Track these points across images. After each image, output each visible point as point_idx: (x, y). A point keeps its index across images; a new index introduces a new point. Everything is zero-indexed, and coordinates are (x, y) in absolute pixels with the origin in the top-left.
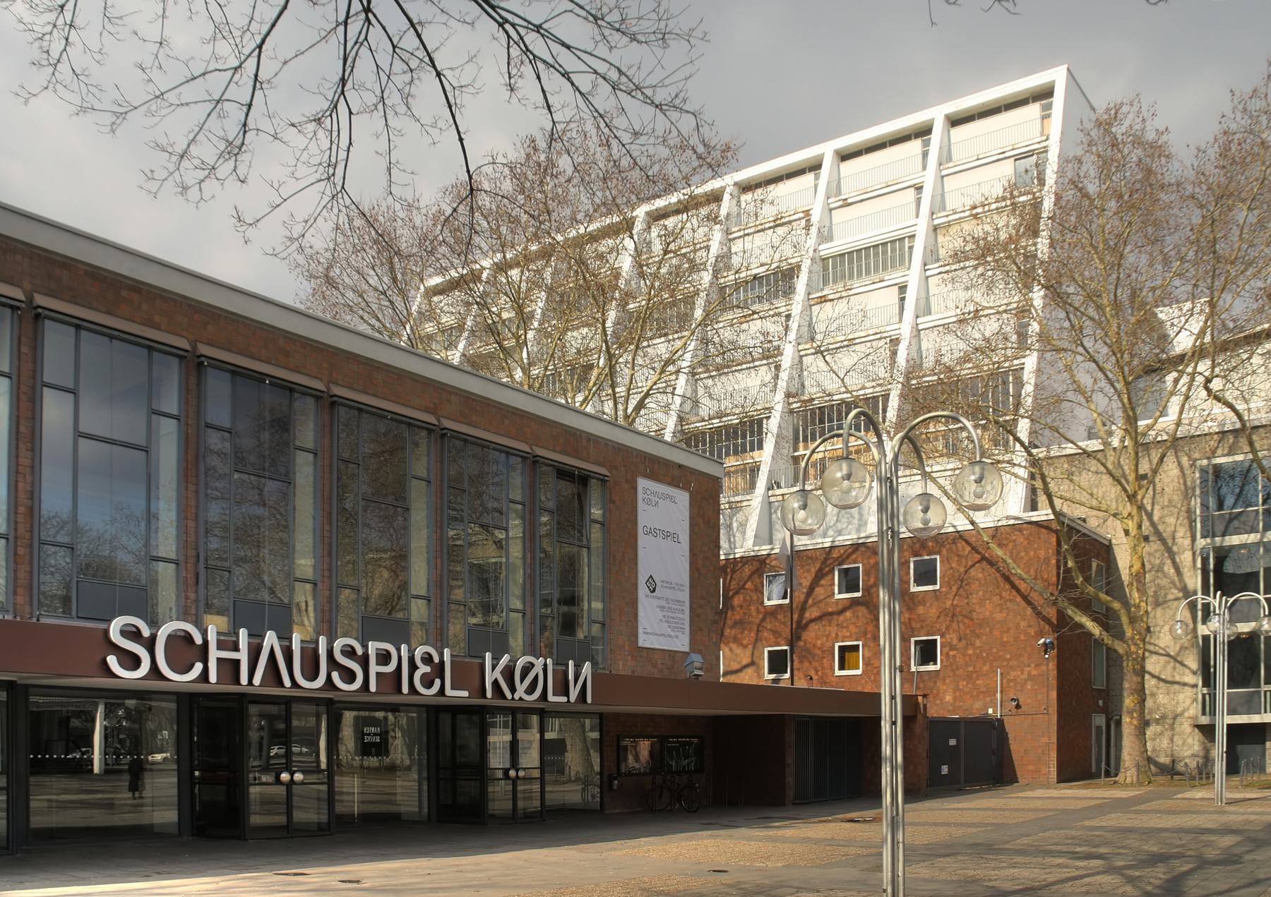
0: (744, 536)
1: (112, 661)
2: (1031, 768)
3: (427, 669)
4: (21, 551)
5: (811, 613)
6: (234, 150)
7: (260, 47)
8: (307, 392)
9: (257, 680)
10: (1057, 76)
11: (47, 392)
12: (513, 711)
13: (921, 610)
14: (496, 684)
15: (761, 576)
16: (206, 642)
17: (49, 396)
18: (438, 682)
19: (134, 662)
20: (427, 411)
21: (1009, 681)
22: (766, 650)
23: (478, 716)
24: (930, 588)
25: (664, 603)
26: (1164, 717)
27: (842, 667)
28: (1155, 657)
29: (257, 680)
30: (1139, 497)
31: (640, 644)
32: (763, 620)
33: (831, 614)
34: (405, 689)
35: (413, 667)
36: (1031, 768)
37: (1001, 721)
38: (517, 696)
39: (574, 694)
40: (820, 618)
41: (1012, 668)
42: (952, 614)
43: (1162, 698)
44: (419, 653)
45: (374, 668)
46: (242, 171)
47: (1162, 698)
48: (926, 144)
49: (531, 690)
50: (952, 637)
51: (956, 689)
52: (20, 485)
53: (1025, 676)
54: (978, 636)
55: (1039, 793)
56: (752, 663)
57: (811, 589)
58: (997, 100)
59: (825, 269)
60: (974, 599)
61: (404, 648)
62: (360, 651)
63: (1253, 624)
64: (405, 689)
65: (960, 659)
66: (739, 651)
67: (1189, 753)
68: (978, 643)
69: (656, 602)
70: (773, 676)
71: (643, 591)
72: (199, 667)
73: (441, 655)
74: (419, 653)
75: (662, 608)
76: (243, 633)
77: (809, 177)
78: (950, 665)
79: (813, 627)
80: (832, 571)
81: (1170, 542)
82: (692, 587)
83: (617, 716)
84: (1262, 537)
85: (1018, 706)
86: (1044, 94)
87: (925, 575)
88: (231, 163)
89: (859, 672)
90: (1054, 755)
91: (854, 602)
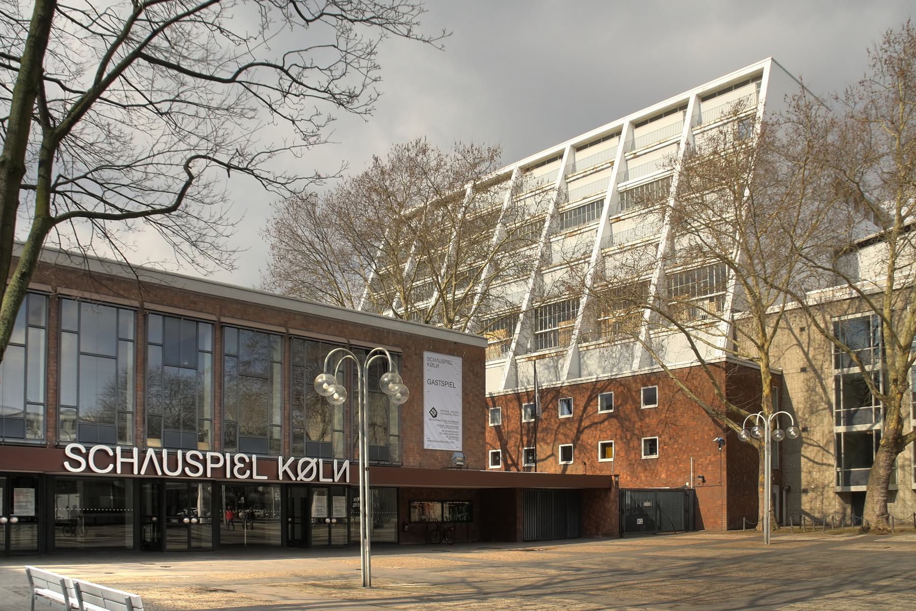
0: (496, 381)
1: (67, 464)
2: (711, 520)
3: (242, 465)
4: (51, 411)
5: (585, 423)
8: (206, 321)
9: (143, 472)
10: (766, 65)
11: (63, 334)
13: (647, 420)
14: (285, 472)
15: (557, 400)
16: (115, 455)
17: (65, 336)
18: (248, 472)
19: (78, 464)
20: (280, 325)
21: (699, 465)
22: (560, 446)
24: (653, 406)
25: (443, 423)
26: (817, 487)
27: (604, 456)
28: (811, 448)
29: (143, 472)
30: (766, 347)
31: (425, 447)
32: (559, 427)
33: (596, 423)
34: (228, 476)
35: (233, 464)
36: (711, 520)
37: (694, 491)
38: (299, 479)
39: (337, 478)
40: (590, 426)
41: (700, 457)
42: (665, 423)
43: (815, 475)
44: (237, 457)
45: (210, 466)
47: (815, 475)
48: (759, 86)
49: (309, 475)
50: (665, 437)
51: (668, 470)
52: (51, 380)
53: (707, 462)
54: (680, 437)
56: (553, 455)
57: (585, 409)
58: (728, 83)
59: (622, 199)
60: (678, 413)
61: (228, 456)
63: (869, 425)
64: (228, 476)
65: (670, 452)
66: (545, 447)
67: (832, 511)
68: (680, 441)
69: (436, 423)
70: (564, 463)
71: (427, 417)
72: (111, 466)
73: (250, 459)
74: (237, 457)
75: (441, 426)
77: (680, 114)
78: (664, 454)
79: (586, 431)
80: (597, 397)
81: (819, 371)
82: (464, 413)
83: (402, 488)
84: (873, 367)
85: (704, 481)
86: (756, 77)
87: (650, 399)
89: (611, 460)
90: (725, 512)
91: (610, 416)
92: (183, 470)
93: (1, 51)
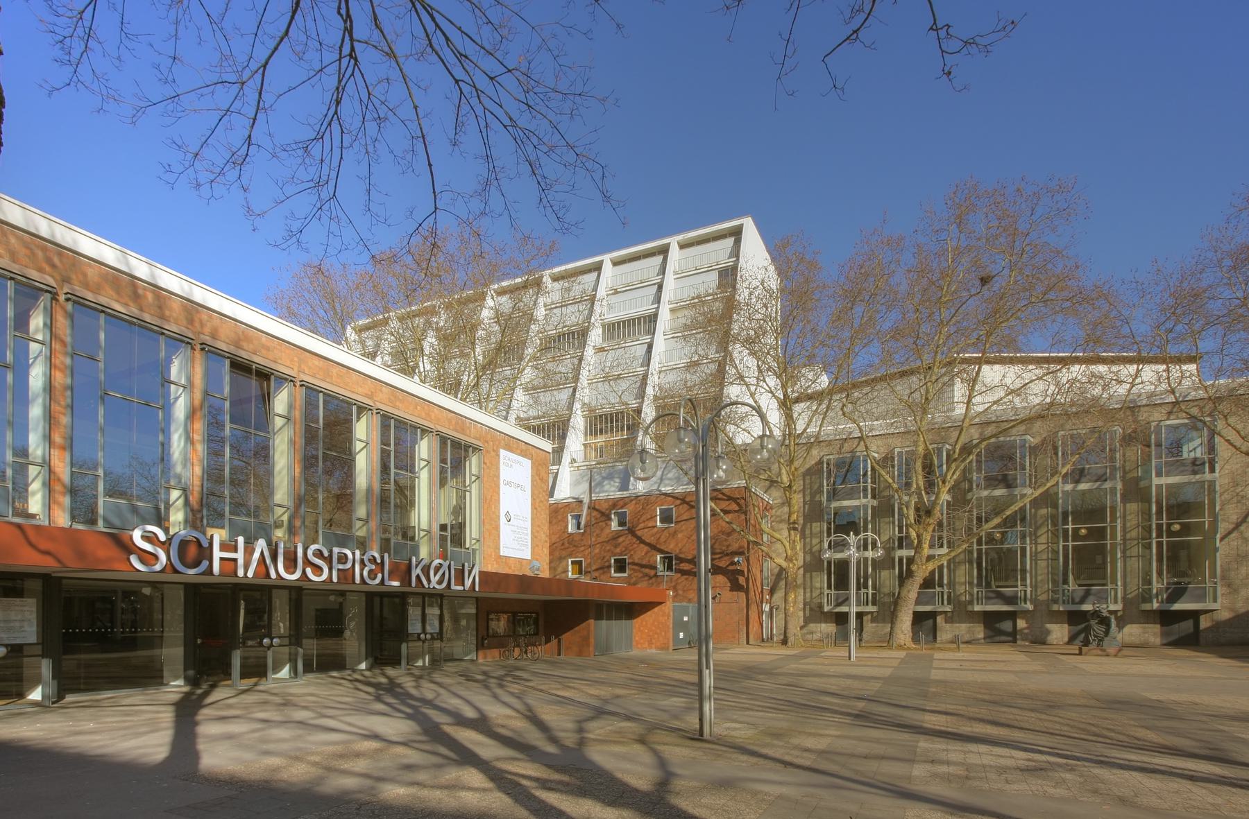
1: (134, 560)
6: (239, 161)
7: (265, 66)
12: (424, 595)
18: (380, 575)
20: (366, 396)
23: (399, 600)
29: (250, 574)
34: (358, 580)
39: (468, 583)
46: (245, 180)
49: (440, 582)
55: (738, 650)
62: (326, 554)
64: (358, 580)
71: (503, 520)
76: (241, 540)
88: (236, 173)
92: (304, 572)
93: (5, 262)
